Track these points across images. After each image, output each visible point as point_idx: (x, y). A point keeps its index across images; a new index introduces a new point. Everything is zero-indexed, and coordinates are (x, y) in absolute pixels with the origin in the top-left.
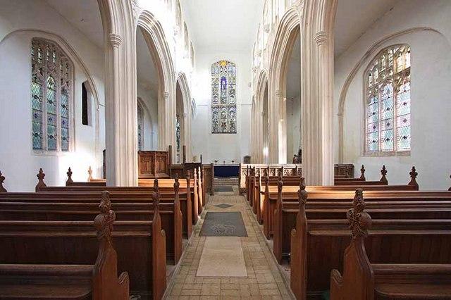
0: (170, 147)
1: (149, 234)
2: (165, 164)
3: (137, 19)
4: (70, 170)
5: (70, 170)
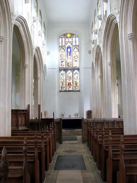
0: (29, 106)
1: (33, 160)
2: (26, 119)
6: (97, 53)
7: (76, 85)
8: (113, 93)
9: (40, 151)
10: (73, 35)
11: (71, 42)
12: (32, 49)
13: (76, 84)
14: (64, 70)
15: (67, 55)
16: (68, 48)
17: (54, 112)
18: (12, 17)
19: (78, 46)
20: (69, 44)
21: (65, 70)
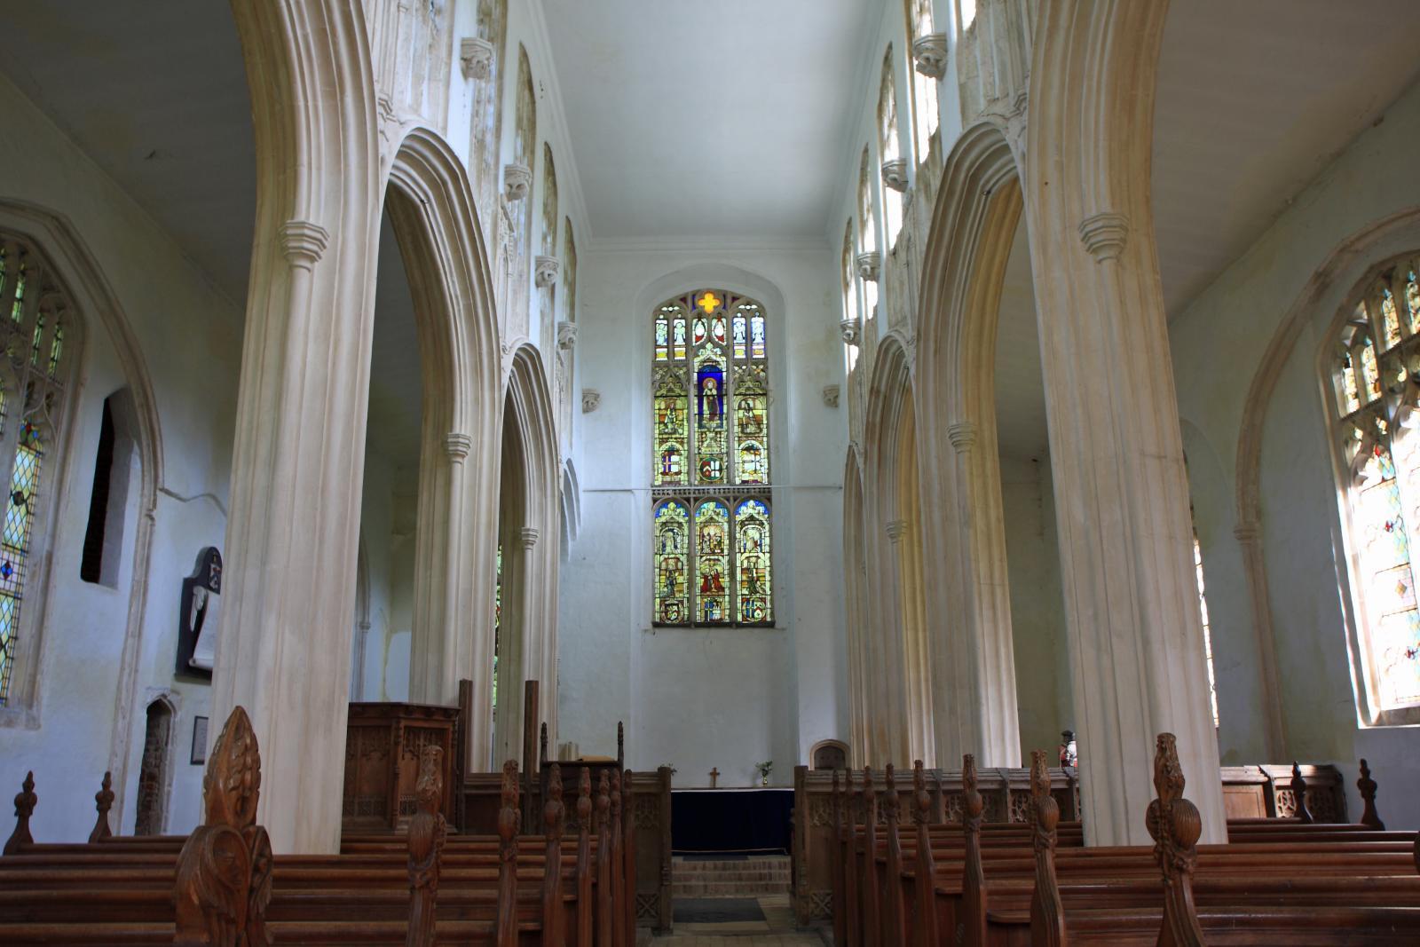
0: (466, 687)
3: (391, 159)
4: (29, 784)
5: (29, 784)
6: (878, 392)
7: (753, 591)
8: (987, 613)
9: (531, 926)
10: (734, 299)
11: (721, 338)
12: (496, 351)
13: (752, 583)
14: (679, 504)
15: (701, 413)
16: (702, 375)
17: (620, 724)
18: (380, 121)
19: (764, 361)
20: (709, 352)
21: (688, 500)
